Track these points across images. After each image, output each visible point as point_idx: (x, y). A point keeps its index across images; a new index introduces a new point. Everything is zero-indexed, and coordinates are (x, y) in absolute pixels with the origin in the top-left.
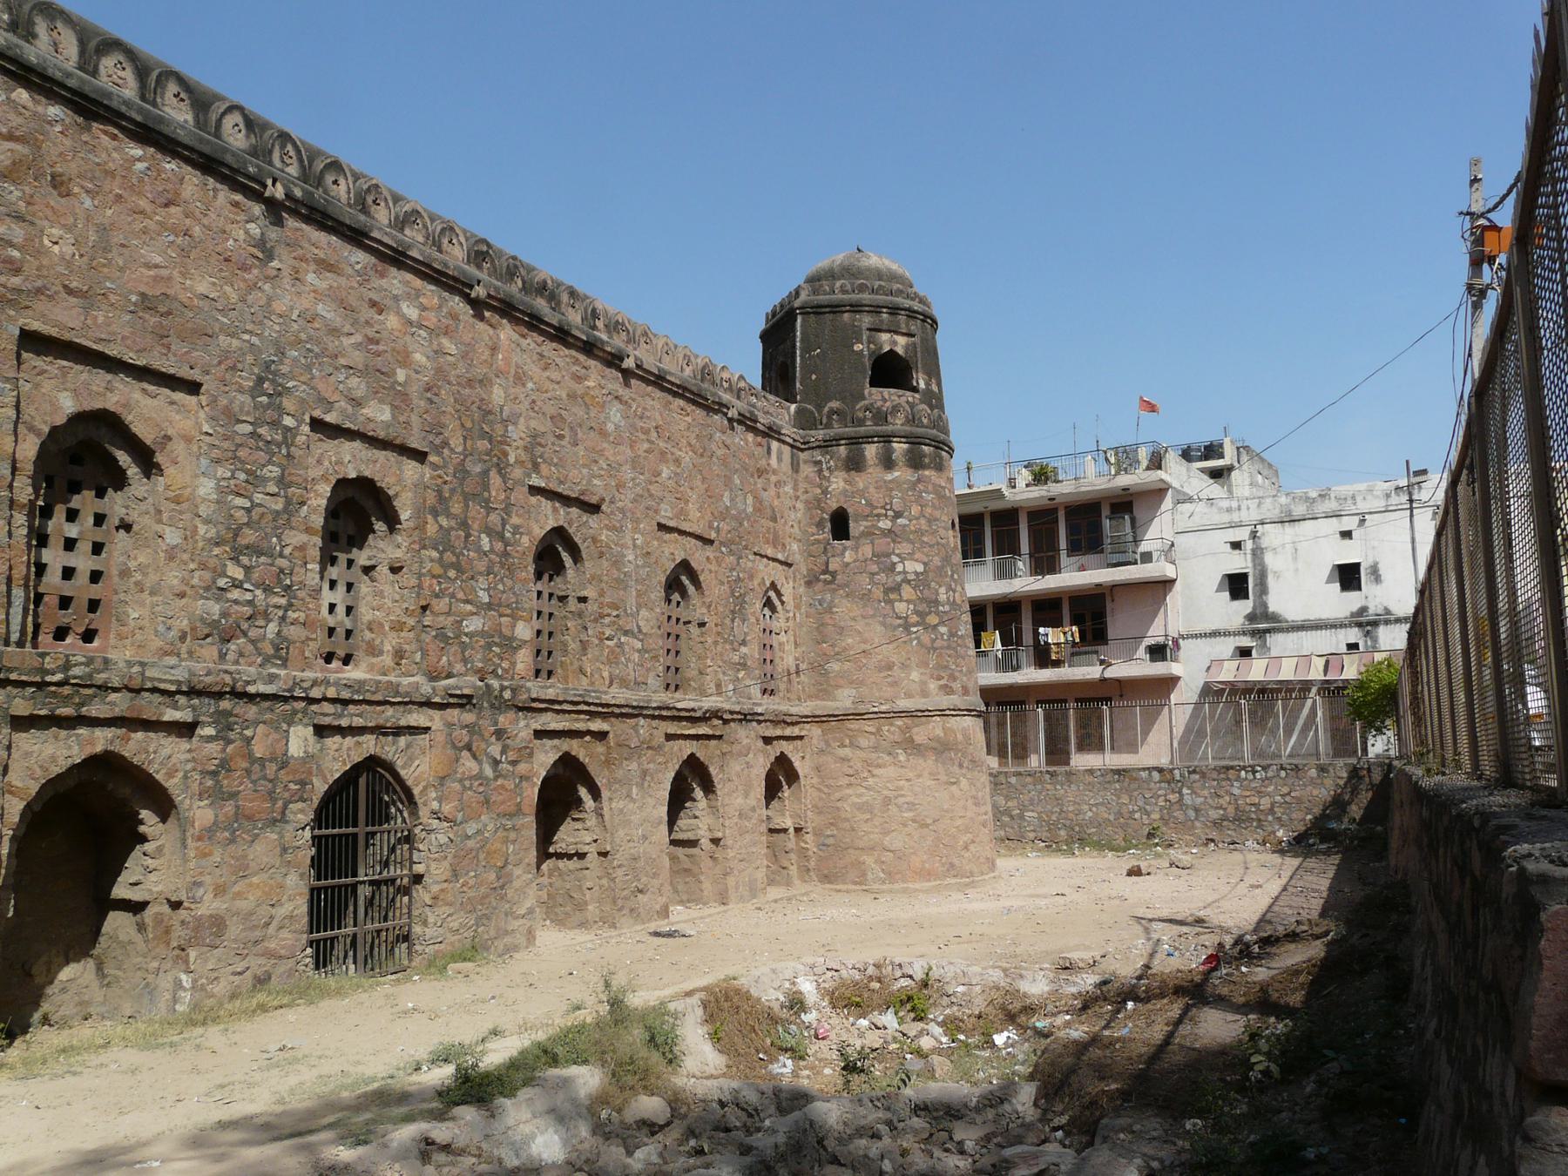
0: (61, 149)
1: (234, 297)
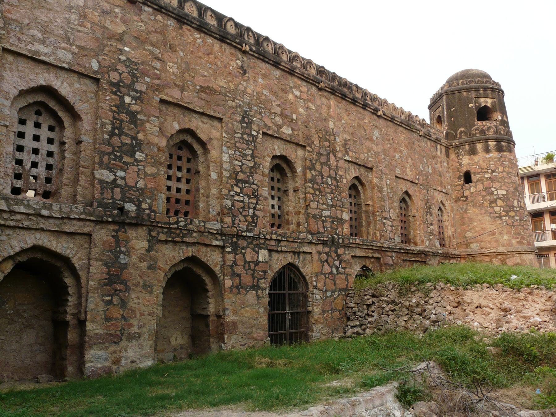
0: (173, 35)
1: (233, 87)
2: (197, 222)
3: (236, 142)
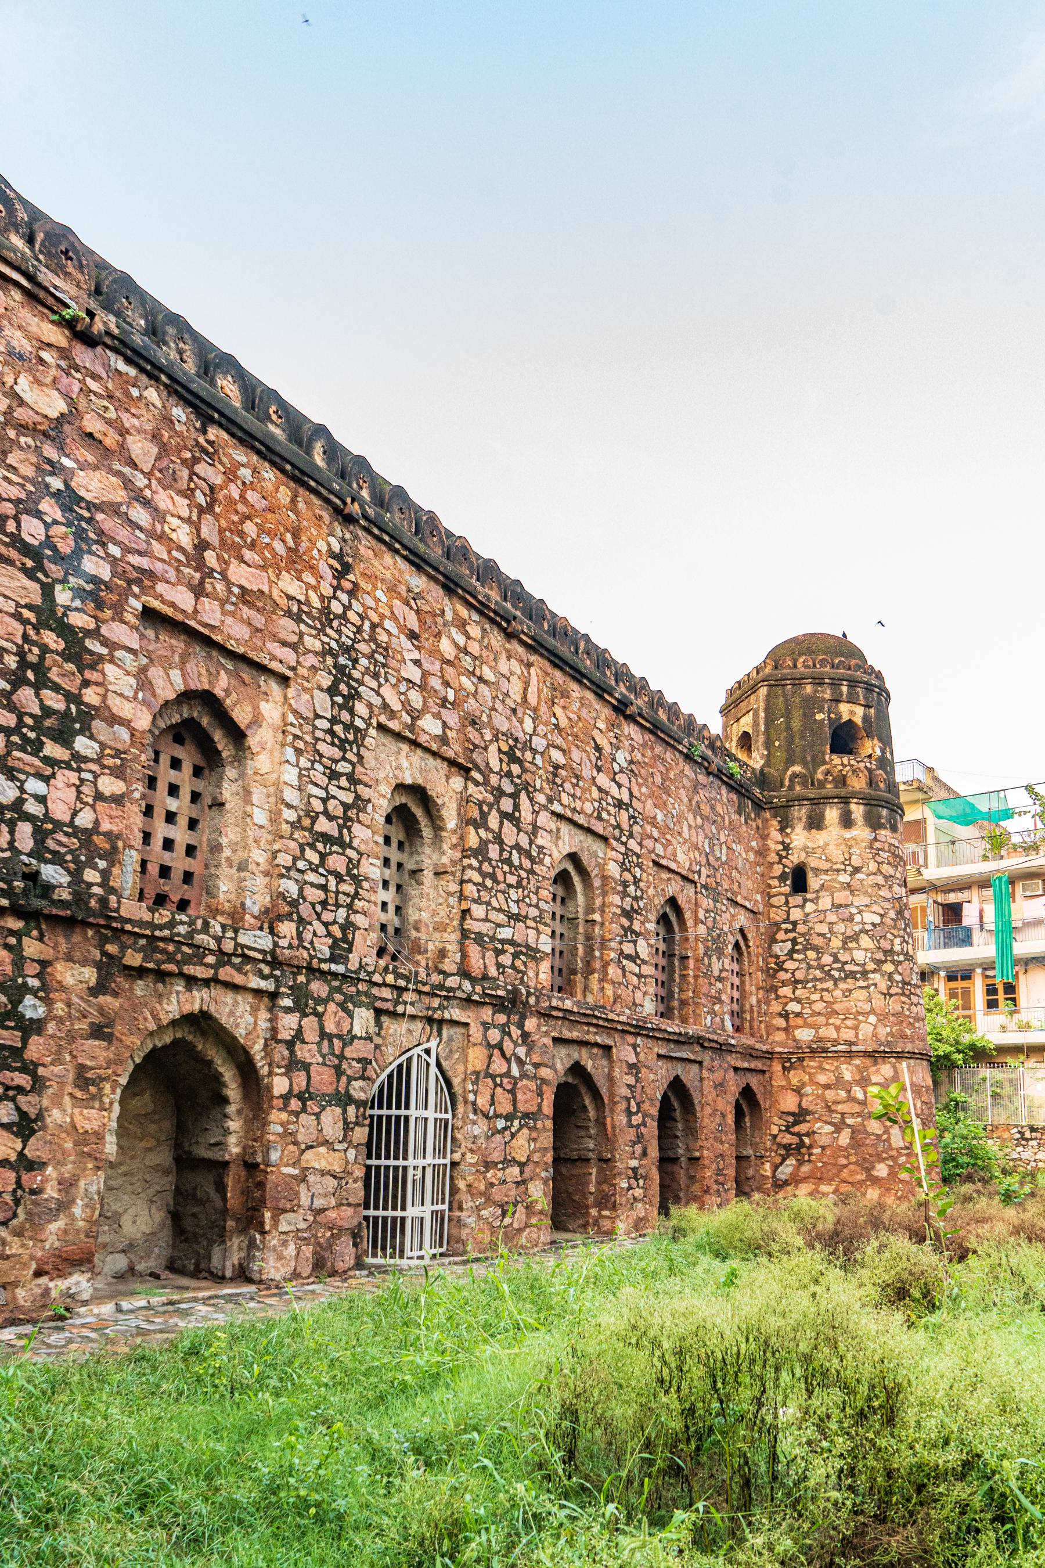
1: (316, 603)
2: (218, 928)
3: (317, 739)
